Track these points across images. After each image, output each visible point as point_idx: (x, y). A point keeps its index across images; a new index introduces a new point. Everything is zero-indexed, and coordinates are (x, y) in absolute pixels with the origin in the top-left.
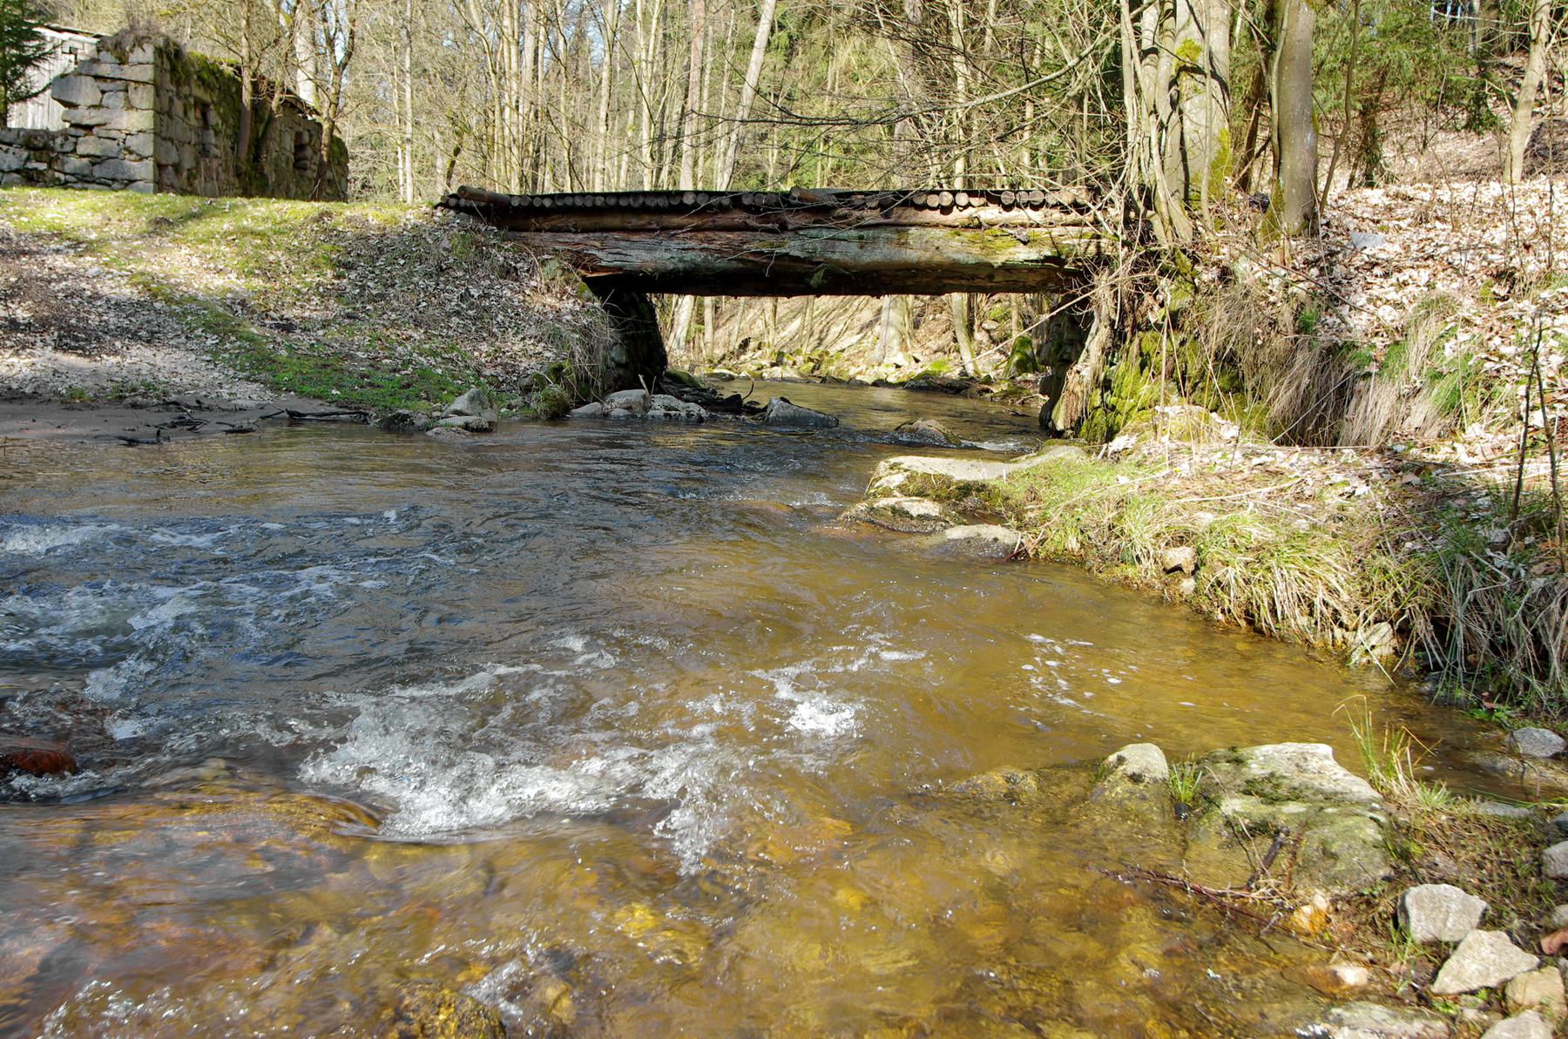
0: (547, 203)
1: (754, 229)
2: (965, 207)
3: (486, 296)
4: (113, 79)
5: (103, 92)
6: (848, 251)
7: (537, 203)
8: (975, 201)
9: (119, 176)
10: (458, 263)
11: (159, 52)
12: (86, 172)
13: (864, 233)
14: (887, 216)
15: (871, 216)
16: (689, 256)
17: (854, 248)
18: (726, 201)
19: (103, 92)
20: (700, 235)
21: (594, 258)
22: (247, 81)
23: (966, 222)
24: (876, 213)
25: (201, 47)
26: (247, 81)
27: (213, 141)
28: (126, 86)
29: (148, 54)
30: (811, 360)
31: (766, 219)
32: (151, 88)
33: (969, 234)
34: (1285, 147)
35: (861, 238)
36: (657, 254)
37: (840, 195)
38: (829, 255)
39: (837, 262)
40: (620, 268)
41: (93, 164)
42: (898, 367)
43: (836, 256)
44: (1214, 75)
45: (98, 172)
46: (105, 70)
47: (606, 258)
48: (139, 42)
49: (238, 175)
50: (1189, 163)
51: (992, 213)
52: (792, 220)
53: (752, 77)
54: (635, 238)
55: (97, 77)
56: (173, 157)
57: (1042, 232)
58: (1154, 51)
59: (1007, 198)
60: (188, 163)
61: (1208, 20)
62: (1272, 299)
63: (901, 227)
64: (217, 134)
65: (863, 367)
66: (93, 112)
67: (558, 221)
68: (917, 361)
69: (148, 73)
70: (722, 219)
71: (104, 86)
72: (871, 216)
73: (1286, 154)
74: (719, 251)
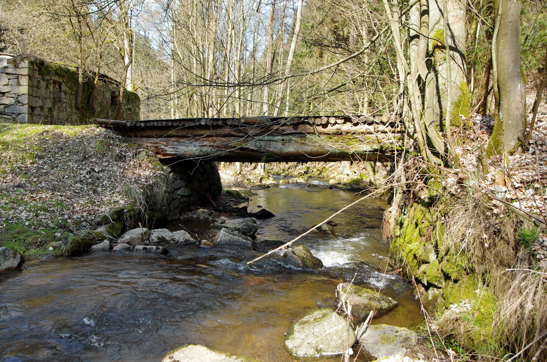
0: (142, 125)
1: (234, 136)
2: (334, 125)
3: (103, 171)
4: (13, 74)
5: (9, 79)
6: (277, 145)
7: (138, 125)
8: (339, 121)
9: (15, 112)
10: (95, 155)
11: (31, 63)
12: (3, 111)
13: (285, 138)
14: (296, 129)
15: (290, 130)
16: (205, 149)
17: (279, 145)
18: (220, 123)
19: (9, 79)
20: (210, 139)
21: (163, 150)
22: (80, 72)
23: (335, 131)
24: (291, 127)
25: (53, 59)
26: (80, 72)
27: (64, 96)
28: (18, 77)
29: (26, 64)
30: (319, 170)
31: (240, 131)
32: (27, 77)
33: (336, 138)
34: (502, 93)
35: (283, 140)
36: (190, 148)
37: (273, 119)
38: (268, 149)
39: (272, 152)
40: (175, 155)
41: (5, 107)
42: (348, 175)
43: (271, 149)
44: (454, 49)
45: (7, 110)
46: (9, 71)
47: (169, 150)
48: (23, 60)
49: (78, 109)
50: (443, 103)
51: (347, 127)
52: (251, 132)
53: (289, 63)
54: (182, 140)
55: (7, 74)
56: (40, 103)
57: (373, 136)
58: (417, 37)
59: (355, 120)
60: (49, 104)
61: (449, 13)
62: (496, 211)
63: (302, 135)
64: (65, 94)
65: (335, 175)
66: (5, 87)
67: (149, 133)
68: (355, 173)
69: (25, 72)
70: (219, 131)
71: (10, 77)
72: (290, 130)
73: (503, 98)
74: (218, 147)
